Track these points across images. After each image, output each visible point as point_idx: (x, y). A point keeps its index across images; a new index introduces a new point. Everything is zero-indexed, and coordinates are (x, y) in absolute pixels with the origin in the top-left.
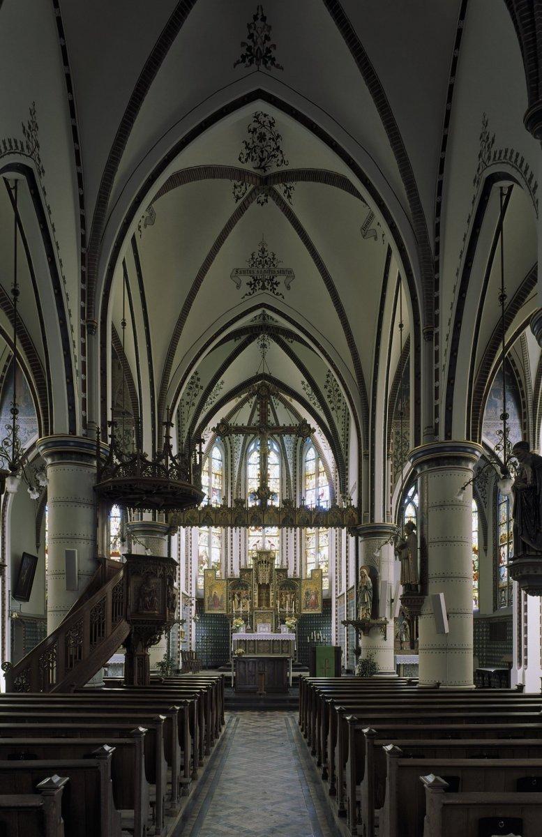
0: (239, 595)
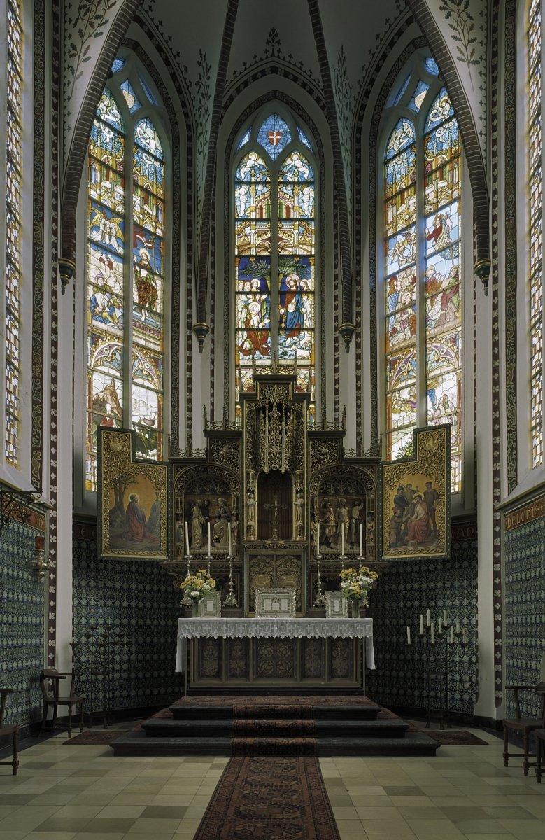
0: (205, 509)
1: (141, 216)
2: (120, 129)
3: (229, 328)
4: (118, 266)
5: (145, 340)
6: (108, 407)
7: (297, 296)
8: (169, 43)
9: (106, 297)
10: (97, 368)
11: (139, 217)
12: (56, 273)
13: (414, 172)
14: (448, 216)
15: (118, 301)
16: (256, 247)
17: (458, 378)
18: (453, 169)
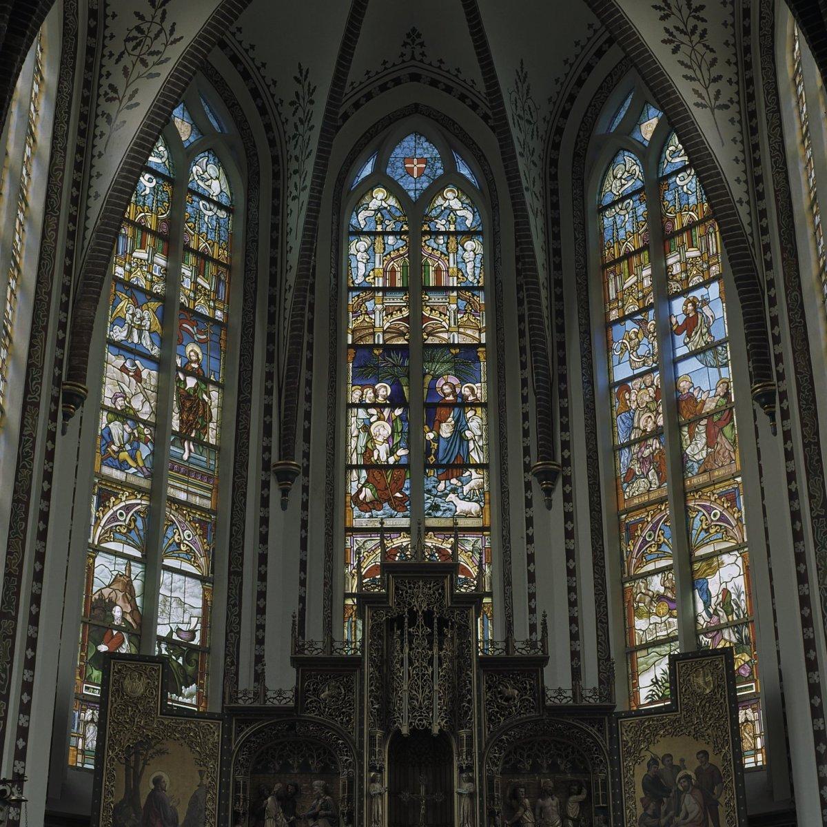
1: (192, 295)
2: (167, 173)
3: (336, 466)
4: (150, 374)
5: (187, 491)
6: (117, 612)
7: (456, 410)
8: (251, 51)
9: (126, 427)
10: (102, 545)
11: (188, 297)
12: (57, 404)
13: (646, 230)
14: (706, 302)
15: (146, 431)
16: (384, 332)
17: (744, 562)
18: (707, 234)
